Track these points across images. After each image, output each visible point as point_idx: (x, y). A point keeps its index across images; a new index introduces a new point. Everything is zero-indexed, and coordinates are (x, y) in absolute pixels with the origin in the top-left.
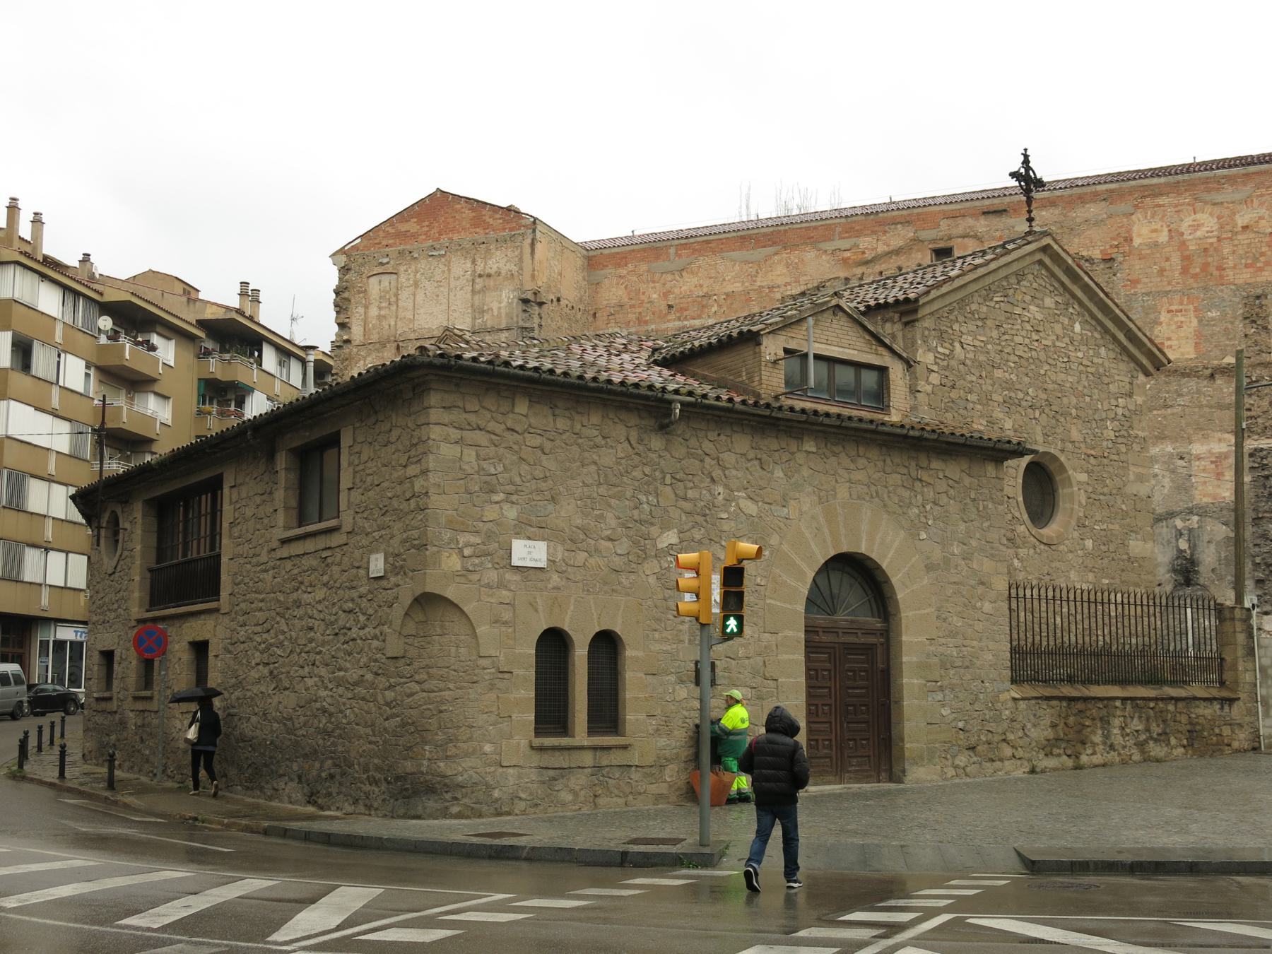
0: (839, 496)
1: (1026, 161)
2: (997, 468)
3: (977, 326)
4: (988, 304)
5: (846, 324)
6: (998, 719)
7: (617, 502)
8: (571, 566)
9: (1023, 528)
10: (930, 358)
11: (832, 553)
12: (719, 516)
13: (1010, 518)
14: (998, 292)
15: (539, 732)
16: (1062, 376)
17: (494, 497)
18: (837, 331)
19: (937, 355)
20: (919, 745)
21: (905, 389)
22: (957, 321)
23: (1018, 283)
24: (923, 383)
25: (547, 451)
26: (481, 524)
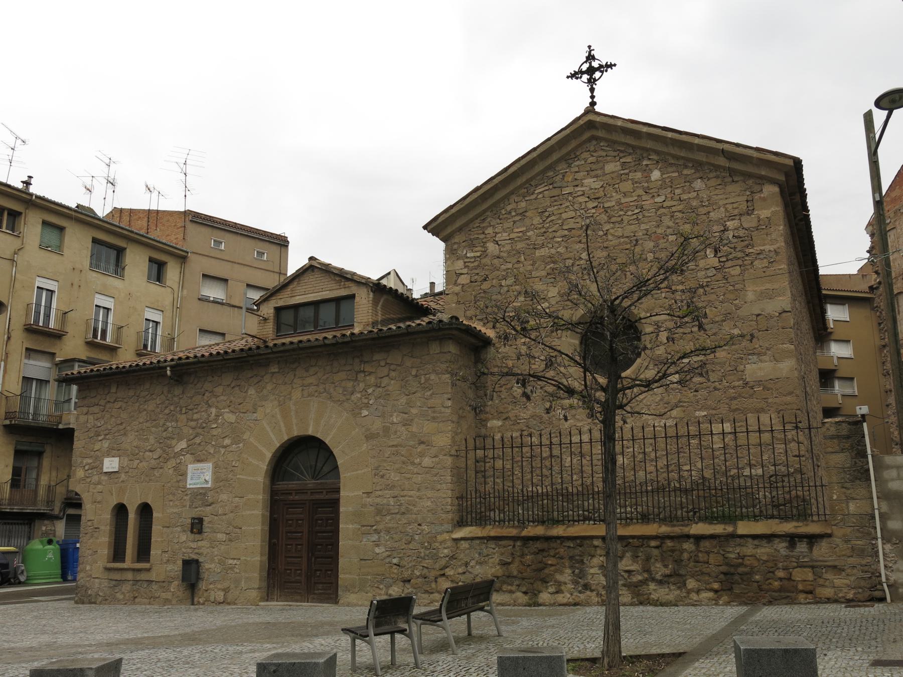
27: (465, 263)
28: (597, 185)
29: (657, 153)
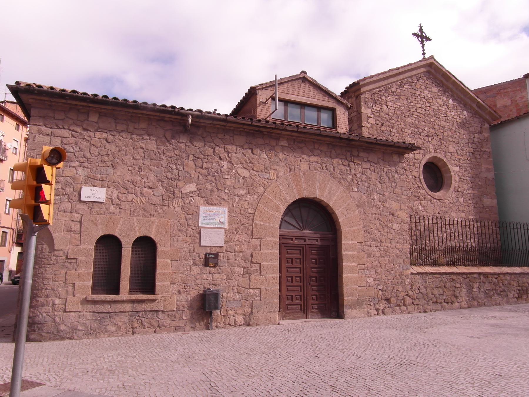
0: (302, 168)
1: (421, 30)
2: (399, 157)
3: (396, 99)
4: (401, 88)
5: (309, 87)
6: (403, 284)
7: (156, 168)
8: (123, 201)
9: (425, 190)
10: (369, 111)
11: (297, 197)
12: (223, 177)
13: (417, 187)
14: (406, 84)
15: (94, 291)
16: (443, 123)
17: (72, 164)
18: (304, 89)
19: (373, 110)
20: (353, 298)
21: (345, 119)
22: (384, 95)
23: (418, 80)
24: (365, 122)
25: (109, 140)
26: (62, 178)
27: (372, 111)
28: (429, 95)
29: (452, 91)
